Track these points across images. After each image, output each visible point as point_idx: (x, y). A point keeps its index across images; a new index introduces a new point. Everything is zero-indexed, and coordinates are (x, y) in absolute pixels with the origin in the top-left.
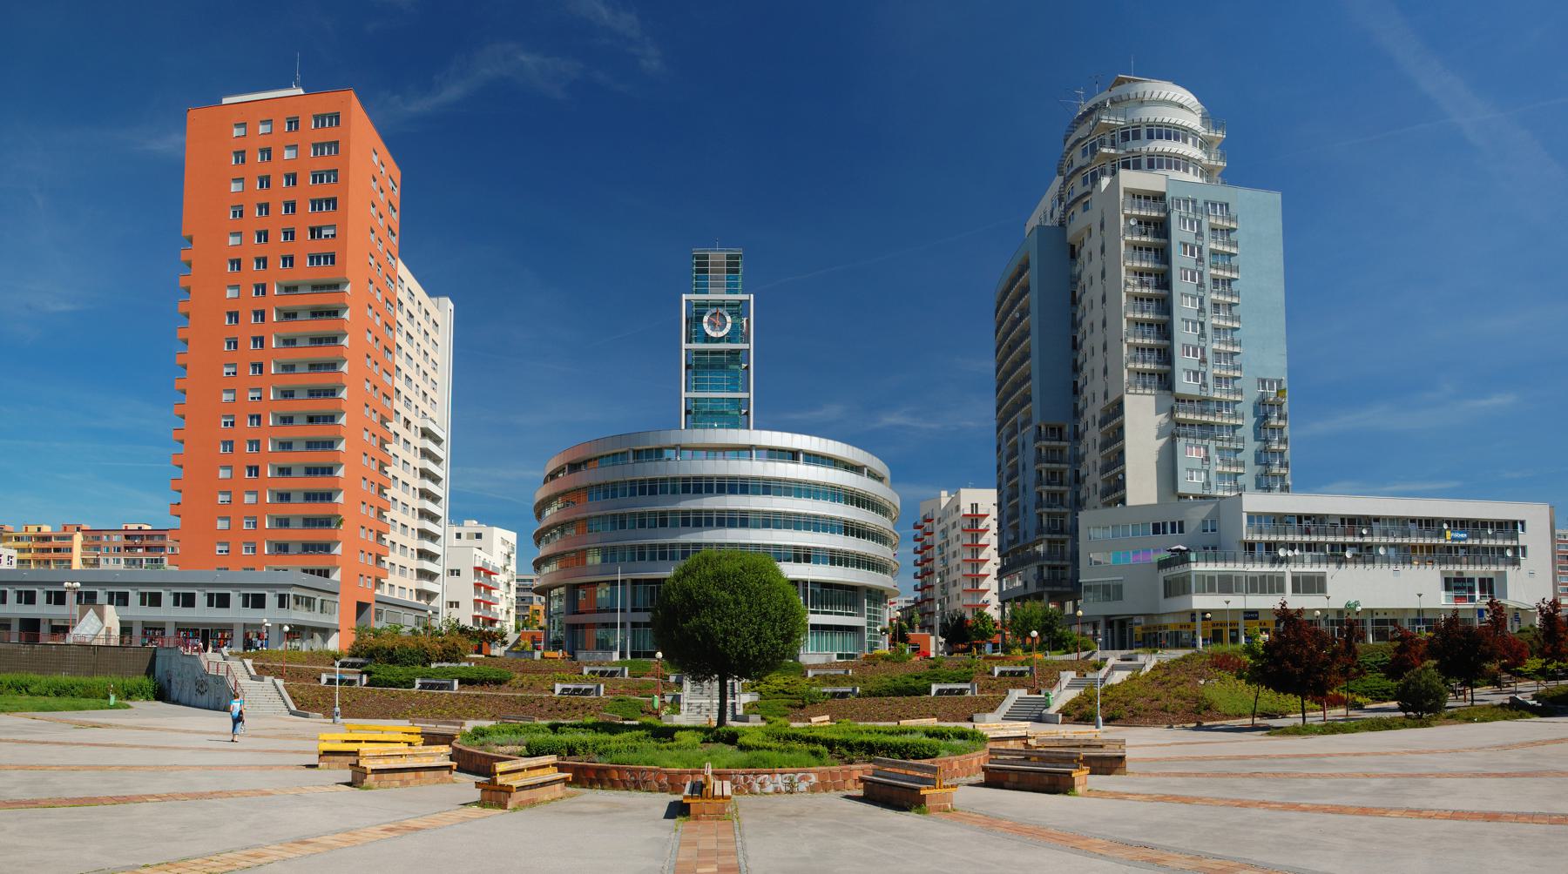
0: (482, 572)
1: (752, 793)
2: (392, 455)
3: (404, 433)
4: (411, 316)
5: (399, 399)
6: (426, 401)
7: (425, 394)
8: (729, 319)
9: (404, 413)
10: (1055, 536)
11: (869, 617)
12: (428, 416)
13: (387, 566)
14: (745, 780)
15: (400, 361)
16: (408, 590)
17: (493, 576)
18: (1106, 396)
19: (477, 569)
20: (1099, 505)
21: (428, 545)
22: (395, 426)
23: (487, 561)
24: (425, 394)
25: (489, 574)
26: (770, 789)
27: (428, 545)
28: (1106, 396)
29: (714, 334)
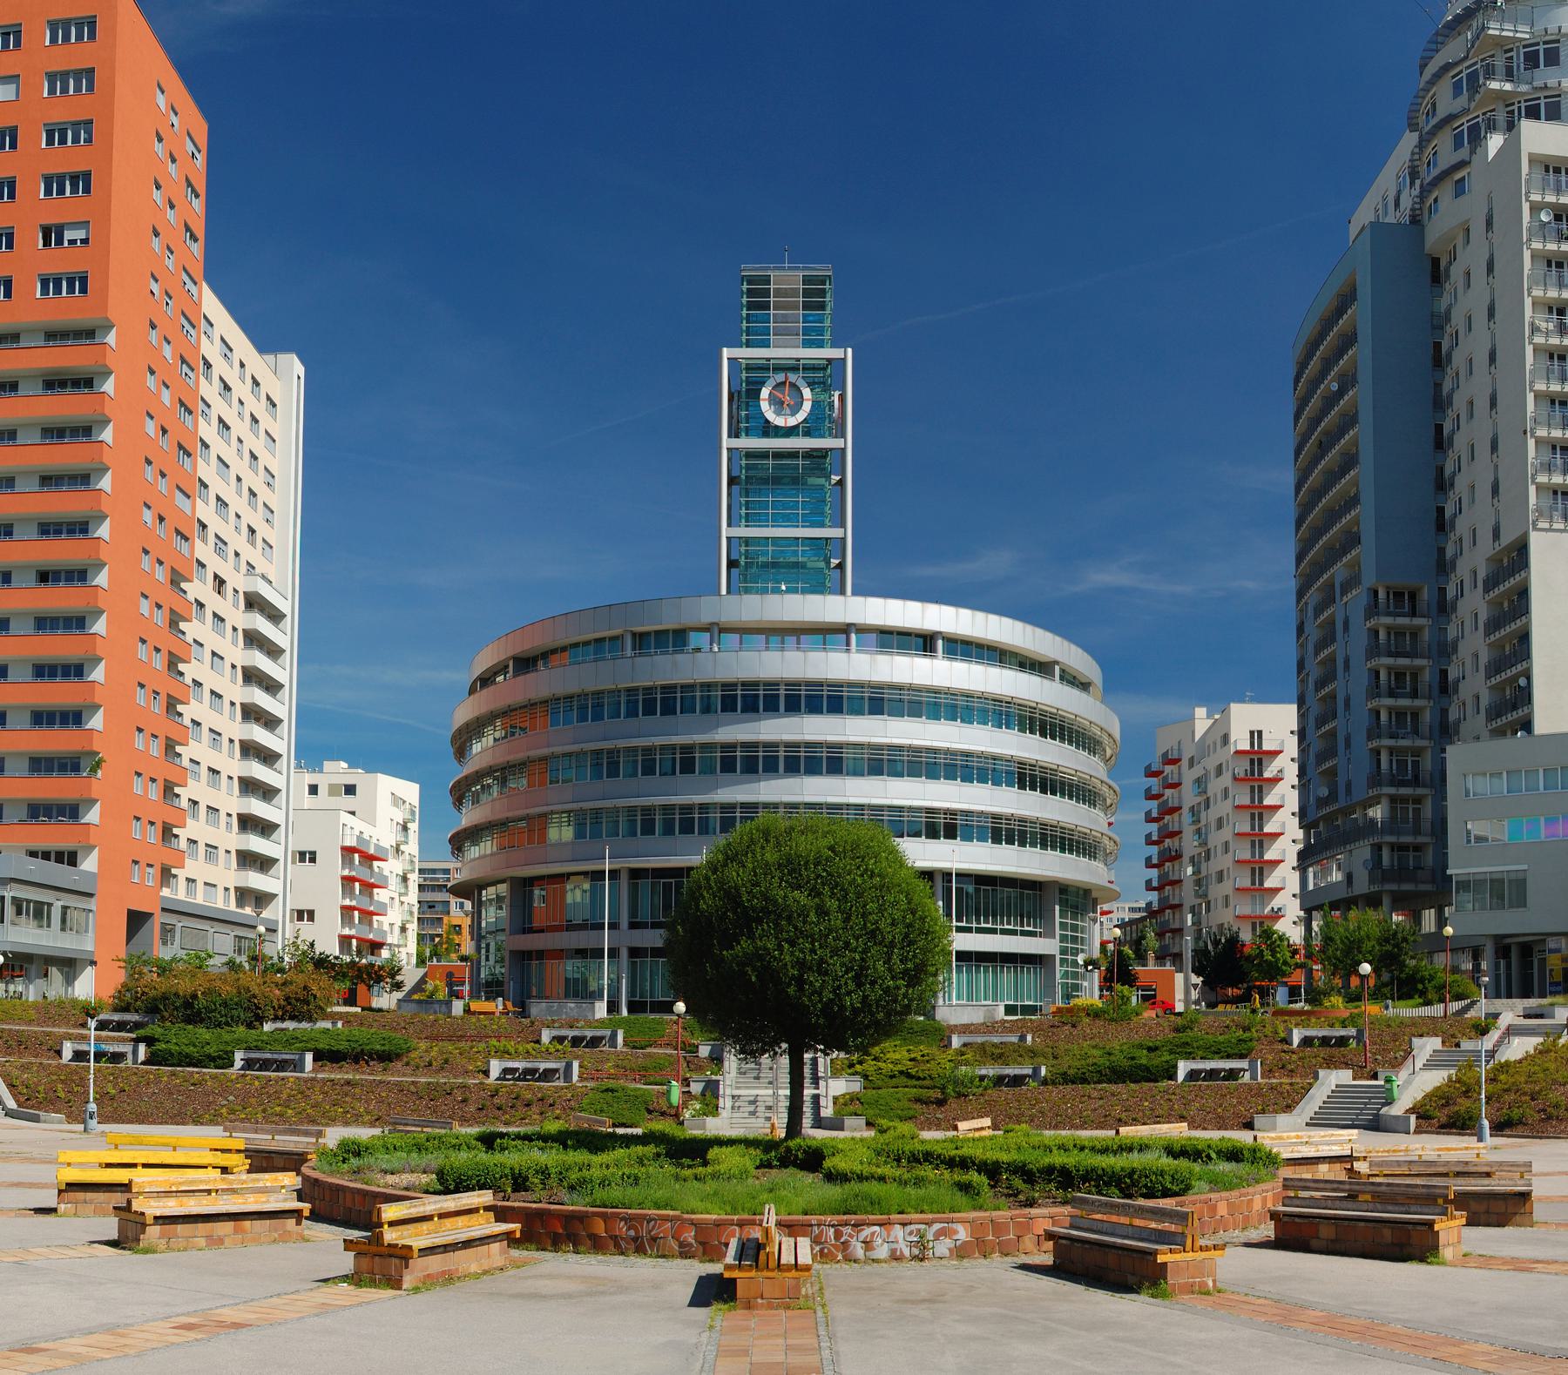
0: (356, 856)
1: (849, 1259)
2: (191, 642)
3: (213, 602)
4: (227, 388)
5: (205, 540)
6: (253, 543)
7: (252, 531)
8: (807, 393)
9: (215, 564)
10: (1404, 791)
11: (1063, 938)
12: (258, 571)
13: (183, 845)
14: (838, 1235)
15: (206, 470)
16: (220, 891)
17: (376, 864)
18: (1496, 534)
19: (348, 851)
20: (1485, 733)
21: (257, 807)
22: (197, 589)
23: (366, 836)
24: (252, 531)
25: (368, 859)
26: (882, 1252)
27: (257, 807)
28: (1496, 534)
29: (779, 421)
